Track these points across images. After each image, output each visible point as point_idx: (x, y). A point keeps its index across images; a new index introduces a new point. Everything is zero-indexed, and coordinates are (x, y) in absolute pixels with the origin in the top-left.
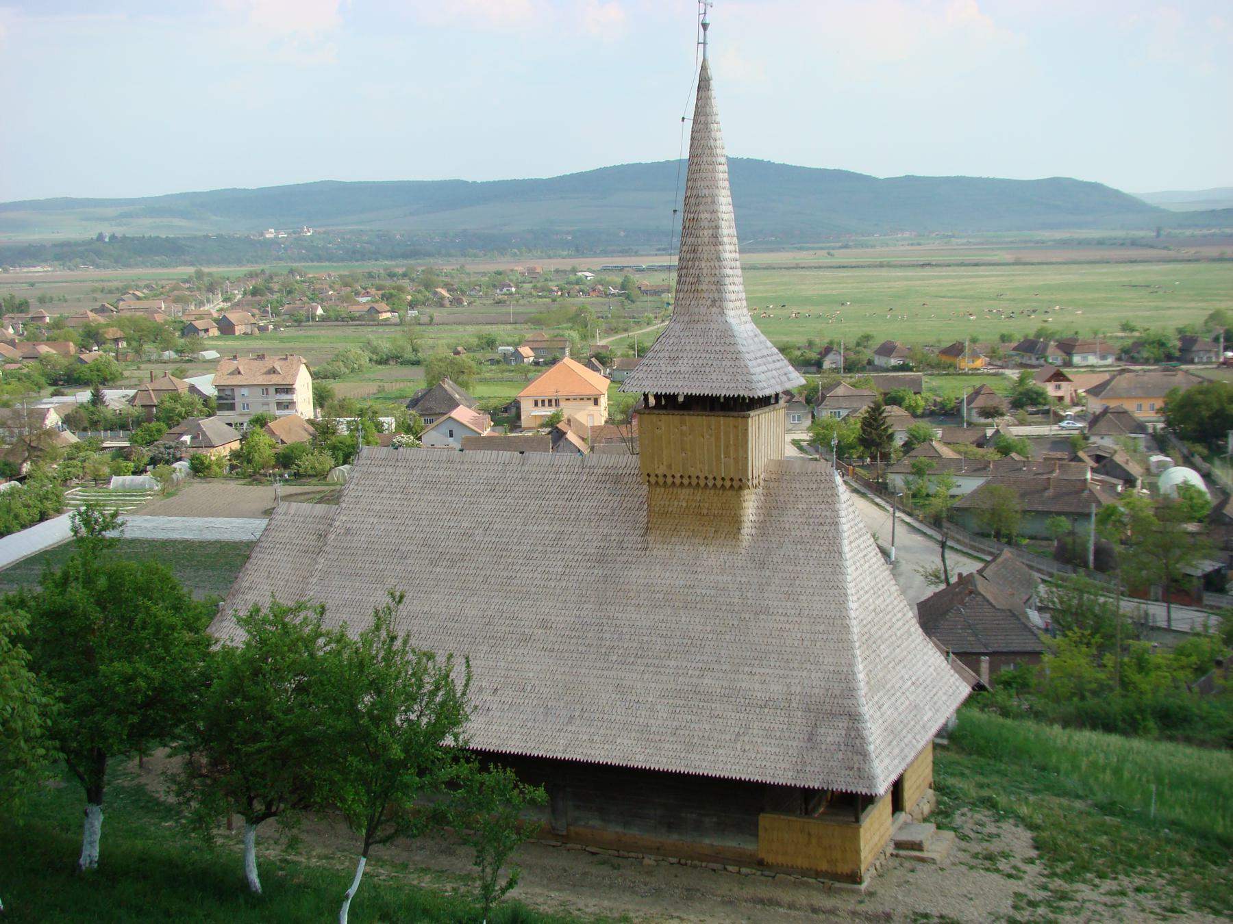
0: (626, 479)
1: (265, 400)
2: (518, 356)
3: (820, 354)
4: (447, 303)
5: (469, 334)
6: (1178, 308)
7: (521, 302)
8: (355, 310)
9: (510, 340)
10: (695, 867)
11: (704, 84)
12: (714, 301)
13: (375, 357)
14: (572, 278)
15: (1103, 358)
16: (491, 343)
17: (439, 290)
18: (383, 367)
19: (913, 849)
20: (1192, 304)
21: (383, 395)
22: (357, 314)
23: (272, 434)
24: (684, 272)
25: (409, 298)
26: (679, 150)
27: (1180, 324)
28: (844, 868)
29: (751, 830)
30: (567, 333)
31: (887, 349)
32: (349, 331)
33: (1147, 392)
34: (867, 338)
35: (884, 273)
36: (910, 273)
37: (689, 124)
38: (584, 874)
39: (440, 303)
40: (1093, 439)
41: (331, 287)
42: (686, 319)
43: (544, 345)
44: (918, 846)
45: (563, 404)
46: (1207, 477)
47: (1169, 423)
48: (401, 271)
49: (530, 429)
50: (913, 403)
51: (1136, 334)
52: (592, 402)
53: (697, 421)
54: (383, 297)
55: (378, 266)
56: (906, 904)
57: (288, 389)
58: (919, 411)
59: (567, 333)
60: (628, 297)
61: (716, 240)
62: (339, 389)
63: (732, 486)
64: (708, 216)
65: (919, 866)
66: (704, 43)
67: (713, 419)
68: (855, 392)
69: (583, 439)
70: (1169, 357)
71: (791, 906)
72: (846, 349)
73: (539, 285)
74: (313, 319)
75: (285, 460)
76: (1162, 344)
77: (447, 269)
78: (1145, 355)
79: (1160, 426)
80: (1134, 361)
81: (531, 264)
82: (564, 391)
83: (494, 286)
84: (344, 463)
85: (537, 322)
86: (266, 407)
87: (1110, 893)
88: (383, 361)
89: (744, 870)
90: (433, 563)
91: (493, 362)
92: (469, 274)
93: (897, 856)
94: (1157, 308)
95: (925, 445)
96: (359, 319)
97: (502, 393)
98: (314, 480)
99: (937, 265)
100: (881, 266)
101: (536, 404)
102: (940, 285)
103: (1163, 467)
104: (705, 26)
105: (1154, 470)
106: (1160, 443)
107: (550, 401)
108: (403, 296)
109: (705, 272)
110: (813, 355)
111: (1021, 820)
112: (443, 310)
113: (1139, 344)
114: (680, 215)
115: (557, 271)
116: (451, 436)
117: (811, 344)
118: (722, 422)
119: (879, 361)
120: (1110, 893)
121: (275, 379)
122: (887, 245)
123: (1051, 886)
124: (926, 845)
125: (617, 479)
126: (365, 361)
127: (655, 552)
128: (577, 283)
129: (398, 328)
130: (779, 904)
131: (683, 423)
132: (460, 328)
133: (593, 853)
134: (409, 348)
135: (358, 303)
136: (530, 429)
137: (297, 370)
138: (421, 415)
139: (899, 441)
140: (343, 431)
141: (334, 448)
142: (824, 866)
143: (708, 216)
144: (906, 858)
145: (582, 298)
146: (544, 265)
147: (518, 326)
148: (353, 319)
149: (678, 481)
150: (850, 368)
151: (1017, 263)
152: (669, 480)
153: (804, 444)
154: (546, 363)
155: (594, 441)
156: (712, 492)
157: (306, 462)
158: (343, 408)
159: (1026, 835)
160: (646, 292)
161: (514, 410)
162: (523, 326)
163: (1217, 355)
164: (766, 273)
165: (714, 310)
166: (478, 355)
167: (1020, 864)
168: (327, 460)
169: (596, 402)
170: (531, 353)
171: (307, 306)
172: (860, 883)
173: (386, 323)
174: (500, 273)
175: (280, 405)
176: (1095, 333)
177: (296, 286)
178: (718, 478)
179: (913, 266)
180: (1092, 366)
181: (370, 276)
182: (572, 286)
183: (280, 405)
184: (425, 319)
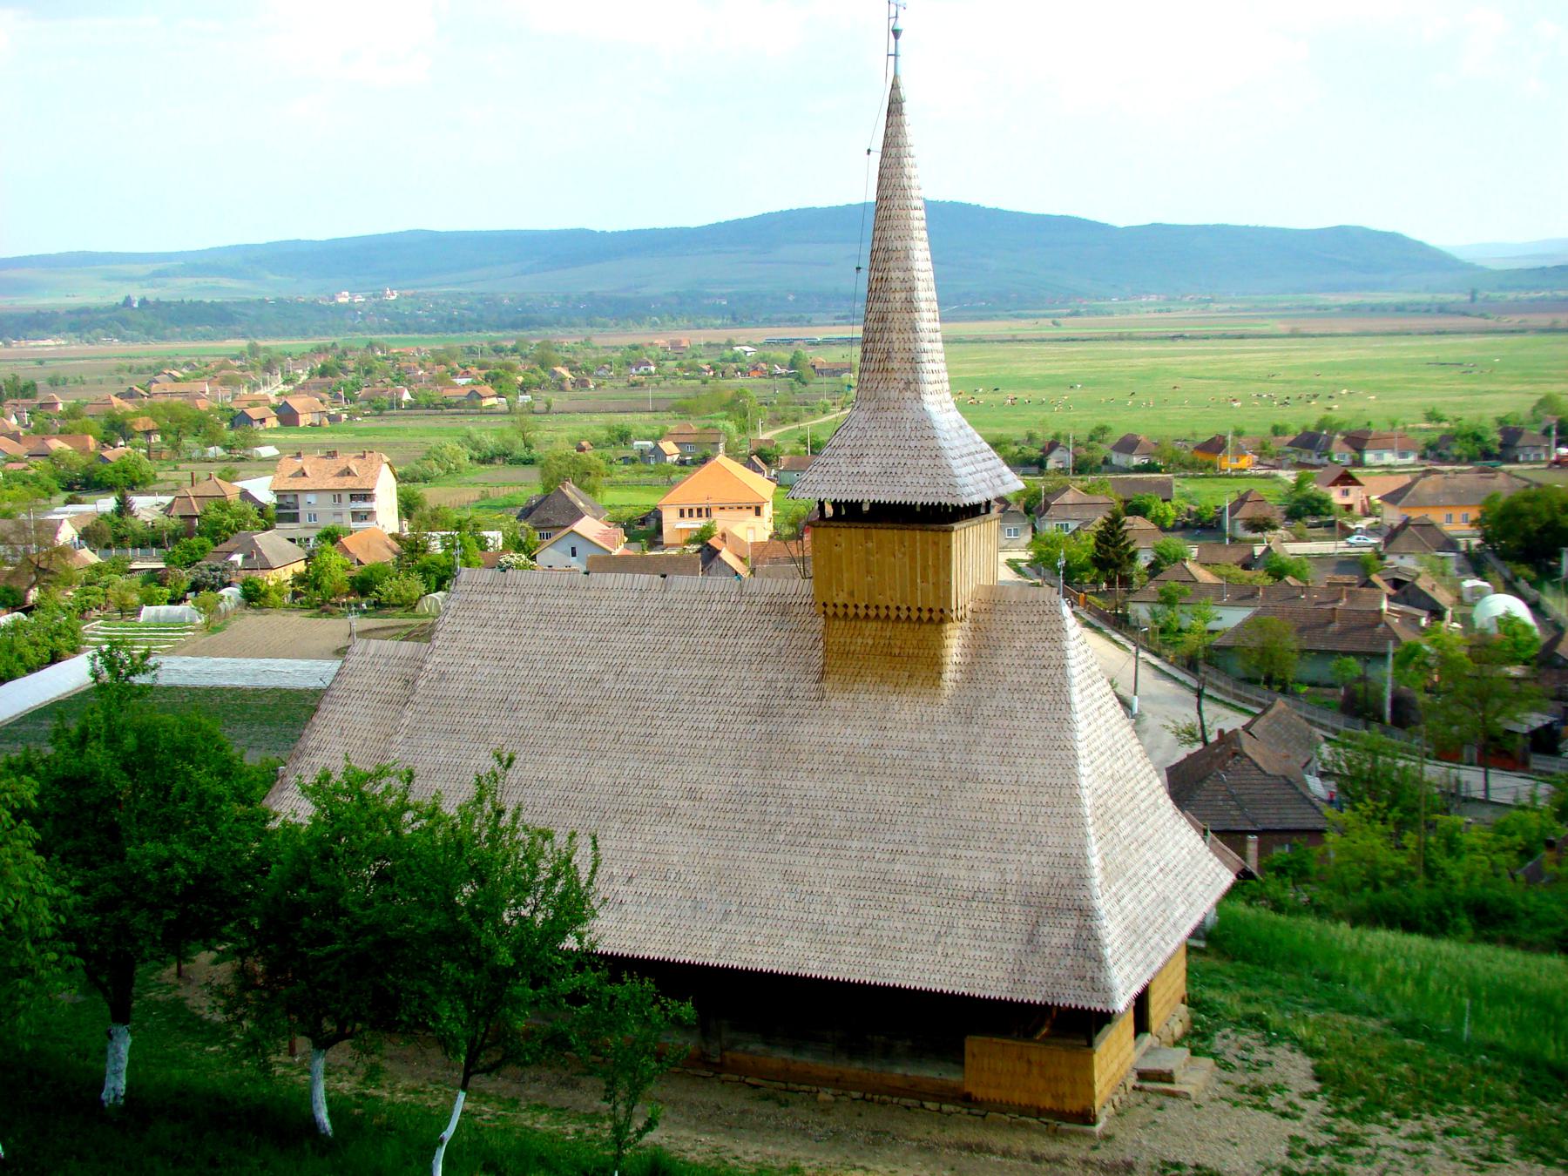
1: (337, 509)
2: (659, 453)
3: (1043, 450)
4: (568, 386)
5: (596, 425)
6: (1497, 392)
7: (663, 384)
8: (451, 394)
9: (648, 432)
10: (883, 1103)
11: (895, 107)
12: (908, 383)
13: (476, 455)
14: (727, 353)
16: (624, 437)
17: (559, 369)
19: (1161, 1080)
20: (1516, 387)
21: (487, 502)
22: (455, 400)
23: (346, 552)
25: (521, 379)
26: (864, 191)
27: (1501, 412)
28: (1073, 1105)
30: (721, 423)
31: (1128, 445)
32: (444, 421)
33: (1459, 499)
34: (1103, 430)
35: (1124, 347)
36: (1157, 347)
37: (876, 157)
40: (1389, 559)
42: (873, 405)
43: (692, 439)
44: (1167, 1077)
45: (716, 514)
46: (1534, 607)
47: (1486, 538)
48: (510, 345)
49: (674, 546)
50: (1161, 513)
52: (753, 512)
53: (888, 536)
55: (481, 339)
56: (1152, 1151)
57: (366, 496)
58: (1169, 524)
59: (721, 423)
60: (799, 378)
61: (910, 305)
62: (432, 495)
63: (930, 619)
64: (901, 275)
66: (896, 55)
67: (907, 534)
69: (741, 559)
70: (1487, 455)
71: (1006, 1153)
72: (1076, 444)
75: (363, 586)
76: (1477, 438)
78: (1456, 451)
79: (1475, 542)
80: (1442, 459)
82: (717, 499)
83: (629, 364)
84: (438, 589)
85: (683, 410)
86: (338, 519)
88: (487, 460)
89: (945, 1107)
90: (551, 716)
91: (627, 460)
93: (1141, 1089)
94: (1472, 393)
96: (456, 406)
98: (400, 612)
99: (1192, 338)
100: (1120, 338)
101: (682, 515)
102: (1196, 363)
103: (1479, 594)
104: (896, 33)
105: (1467, 598)
106: (1476, 564)
107: (699, 510)
108: (512, 376)
109: (896, 346)
110: (1034, 452)
114: (865, 273)
116: (574, 554)
117: (1031, 438)
118: (918, 538)
119: (1117, 459)
121: (350, 482)
122: (1128, 312)
123: (1336, 1128)
124: (1178, 1075)
126: (464, 459)
127: (833, 703)
128: (734, 360)
129: (506, 418)
131: (868, 538)
132: (585, 417)
134: (521, 443)
135: (456, 386)
136: (674, 546)
137: (378, 471)
139: (1143, 561)
140: (436, 548)
141: (425, 570)
142: (1048, 1102)
143: (901, 275)
144: (1152, 1091)
145: (740, 380)
147: (658, 415)
148: (449, 406)
149: (862, 612)
150: (1081, 468)
151: (1293, 335)
153: (1023, 565)
154: (694, 463)
155: (755, 561)
156: (906, 626)
157: (389, 588)
158: (436, 520)
159: (1304, 1063)
160: (821, 372)
161: (653, 522)
162: (665, 415)
163: (1548, 453)
164: (974, 346)
165: (908, 394)
167: (1297, 1100)
169: (758, 512)
170: (676, 450)
172: (1094, 1123)
173: (491, 411)
174: (635, 348)
175: (356, 515)
176: (1393, 424)
177: (377, 364)
178: (872, 607)
179: (1161, 338)
180: (1389, 466)
181: (471, 351)
183: (356, 515)
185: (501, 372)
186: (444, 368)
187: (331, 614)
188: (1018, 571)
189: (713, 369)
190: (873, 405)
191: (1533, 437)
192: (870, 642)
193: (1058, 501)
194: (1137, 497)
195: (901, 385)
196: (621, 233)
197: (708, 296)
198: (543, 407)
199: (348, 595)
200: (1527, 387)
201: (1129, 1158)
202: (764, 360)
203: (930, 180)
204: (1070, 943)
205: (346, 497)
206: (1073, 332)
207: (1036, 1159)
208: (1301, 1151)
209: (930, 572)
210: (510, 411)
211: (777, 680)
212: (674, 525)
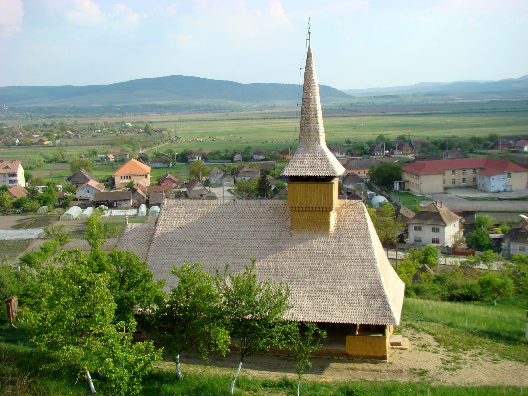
0: (279, 209)
1: (4, 180)
2: (108, 158)
3: (232, 155)
4: (72, 137)
5: (85, 150)
7: (104, 136)
9: (103, 152)
10: (320, 358)
13: (46, 160)
14: (123, 126)
15: (341, 154)
16: (95, 153)
17: (68, 131)
18: (50, 164)
19: (397, 345)
20: (369, 133)
21: (52, 176)
22: (34, 142)
23: (11, 194)
24: (303, 128)
25: (56, 135)
28: (380, 354)
29: (343, 342)
30: (126, 148)
31: (259, 153)
32: (32, 149)
33: (362, 167)
35: (249, 122)
37: (303, 71)
38: (278, 364)
39: (69, 137)
40: (344, 186)
41: (21, 131)
42: (305, 146)
43: (118, 154)
44: (399, 344)
45: (133, 178)
46: (388, 199)
47: (371, 179)
48: (49, 123)
49: (119, 188)
51: (351, 144)
52: (145, 177)
54: (44, 135)
55: (40, 121)
56: (406, 366)
57: (15, 175)
58: (276, 177)
59: (126, 148)
60: (148, 133)
61: (316, 115)
62: (35, 174)
63: (306, 210)
64: (314, 106)
65: (402, 351)
68: (251, 170)
69: (144, 192)
70: (366, 153)
71: (363, 370)
72: (242, 153)
73: (110, 129)
74: (15, 145)
75: (18, 205)
76: (363, 148)
77: (69, 123)
78: (357, 152)
79: (368, 180)
80: (352, 155)
81: (105, 120)
82: (133, 173)
83: (91, 130)
84: (44, 205)
85: (112, 144)
86: (4, 183)
87: (470, 356)
89: (340, 358)
90: (202, 245)
91: (97, 161)
92: (79, 125)
93: (392, 348)
94: (357, 134)
95: (284, 190)
96: (36, 144)
97: (106, 174)
98: (31, 213)
99: (270, 119)
100: (248, 119)
101: (121, 178)
103: (372, 196)
104: (309, 33)
105: (369, 197)
106: (369, 187)
107: (127, 177)
108: (53, 134)
109: (312, 128)
110: (229, 154)
111: (427, 332)
112: (71, 140)
113: (356, 148)
114: (300, 106)
115: (116, 123)
116: (88, 192)
117: (227, 151)
120: (470, 356)
121: (8, 171)
122: (249, 111)
123: (451, 355)
124: (402, 344)
125: (275, 209)
126: (42, 162)
127: (295, 237)
128: (126, 128)
129: (53, 148)
130: (358, 369)
132: (80, 147)
133: (278, 356)
135: (34, 138)
136: (119, 188)
137: (18, 167)
138: (73, 184)
140: (40, 192)
141: (39, 199)
142: (372, 354)
143: (314, 106)
144: (396, 348)
145: (129, 134)
146: (111, 120)
147: (104, 146)
148: (33, 144)
149: (304, 209)
150: (245, 159)
152: (301, 209)
153: (233, 191)
155: (148, 192)
157: (27, 205)
158: (38, 182)
159: (431, 337)
160: (156, 131)
161: (111, 181)
162: (106, 146)
163: (383, 152)
164: (201, 122)
165: (316, 142)
166: (91, 158)
167: (436, 348)
168: (36, 203)
169: (146, 177)
170: (113, 157)
171: (12, 139)
172: (386, 359)
173: (47, 146)
174: (92, 124)
175: (11, 181)
177: (5, 131)
179: (260, 119)
181: (36, 126)
182: (123, 129)
183: (11, 181)
184: (64, 144)
185: (49, 133)
186: (28, 132)
187: (7, 215)
188: (231, 193)
189: (120, 131)
190: (305, 146)
191: (379, 148)
192: (307, 218)
193: (242, 171)
194: (266, 168)
195: (314, 140)
196: (94, 86)
197: (114, 107)
198: (65, 144)
199: (12, 208)
200: (372, 133)
201: (400, 368)
202: (135, 127)
203: (317, 80)
204: (380, 306)
205: (7, 175)
206: (233, 117)
207: (372, 371)
208: (445, 363)
209: (326, 196)
210: (54, 146)
211: (276, 231)
212: (119, 181)
